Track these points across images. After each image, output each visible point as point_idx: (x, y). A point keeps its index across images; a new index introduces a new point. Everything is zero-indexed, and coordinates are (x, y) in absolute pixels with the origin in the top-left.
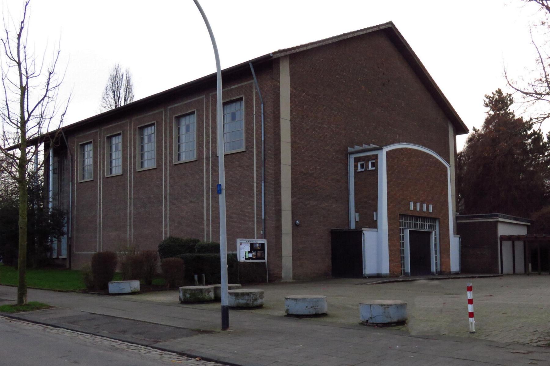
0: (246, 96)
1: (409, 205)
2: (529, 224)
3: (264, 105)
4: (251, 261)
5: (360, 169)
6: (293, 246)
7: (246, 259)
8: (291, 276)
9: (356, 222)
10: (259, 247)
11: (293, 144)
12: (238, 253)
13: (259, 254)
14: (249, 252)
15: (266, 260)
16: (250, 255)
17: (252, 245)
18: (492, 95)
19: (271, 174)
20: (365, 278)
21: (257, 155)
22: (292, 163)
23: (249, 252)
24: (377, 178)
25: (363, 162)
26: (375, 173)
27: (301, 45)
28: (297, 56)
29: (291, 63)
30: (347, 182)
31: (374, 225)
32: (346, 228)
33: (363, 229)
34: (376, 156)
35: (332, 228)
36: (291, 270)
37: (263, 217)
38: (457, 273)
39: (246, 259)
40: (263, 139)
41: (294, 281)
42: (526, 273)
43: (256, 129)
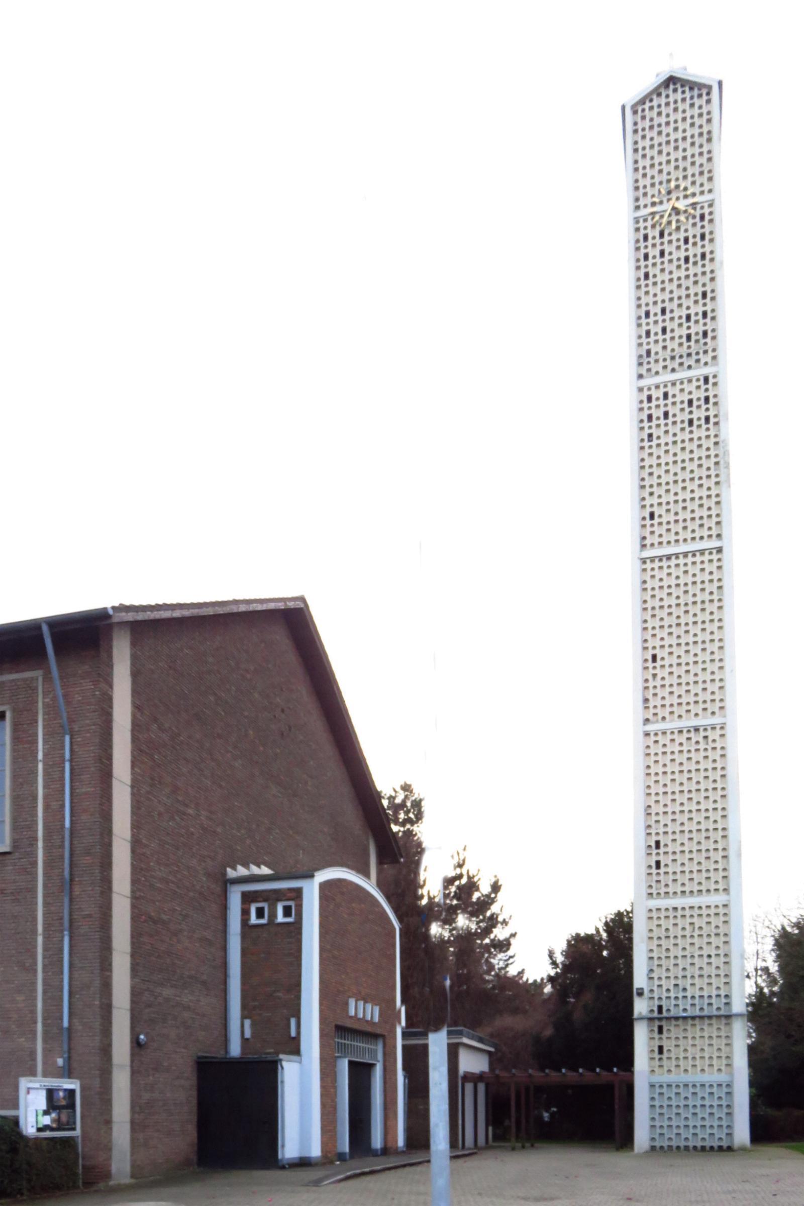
0: (14, 710)
1: (347, 1004)
2: (492, 1049)
3: (71, 739)
4: (48, 1134)
5: (253, 920)
6: (132, 1096)
7: (39, 1130)
8: (128, 1168)
9: (244, 1041)
10: (64, 1098)
11: (136, 843)
12: (21, 1113)
13: (64, 1118)
14: (46, 1113)
15: (77, 1132)
16: (46, 1120)
17: (51, 1094)
18: (393, 794)
19: (90, 916)
20: (283, 1168)
21: (48, 865)
22: (133, 891)
23: (46, 1113)
24: (299, 941)
25: (260, 905)
26: (295, 930)
27: (157, 605)
28: (157, 629)
29: (133, 644)
30: (224, 949)
31: (294, 1047)
32: (220, 1054)
33: (281, 1056)
34: (297, 894)
35: (201, 1054)
36: (128, 1154)
37: (66, 1024)
38: (403, 1152)
39: (39, 1130)
40: (67, 824)
41: (133, 1181)
42: (488, 1147)
43: (46, 797)
